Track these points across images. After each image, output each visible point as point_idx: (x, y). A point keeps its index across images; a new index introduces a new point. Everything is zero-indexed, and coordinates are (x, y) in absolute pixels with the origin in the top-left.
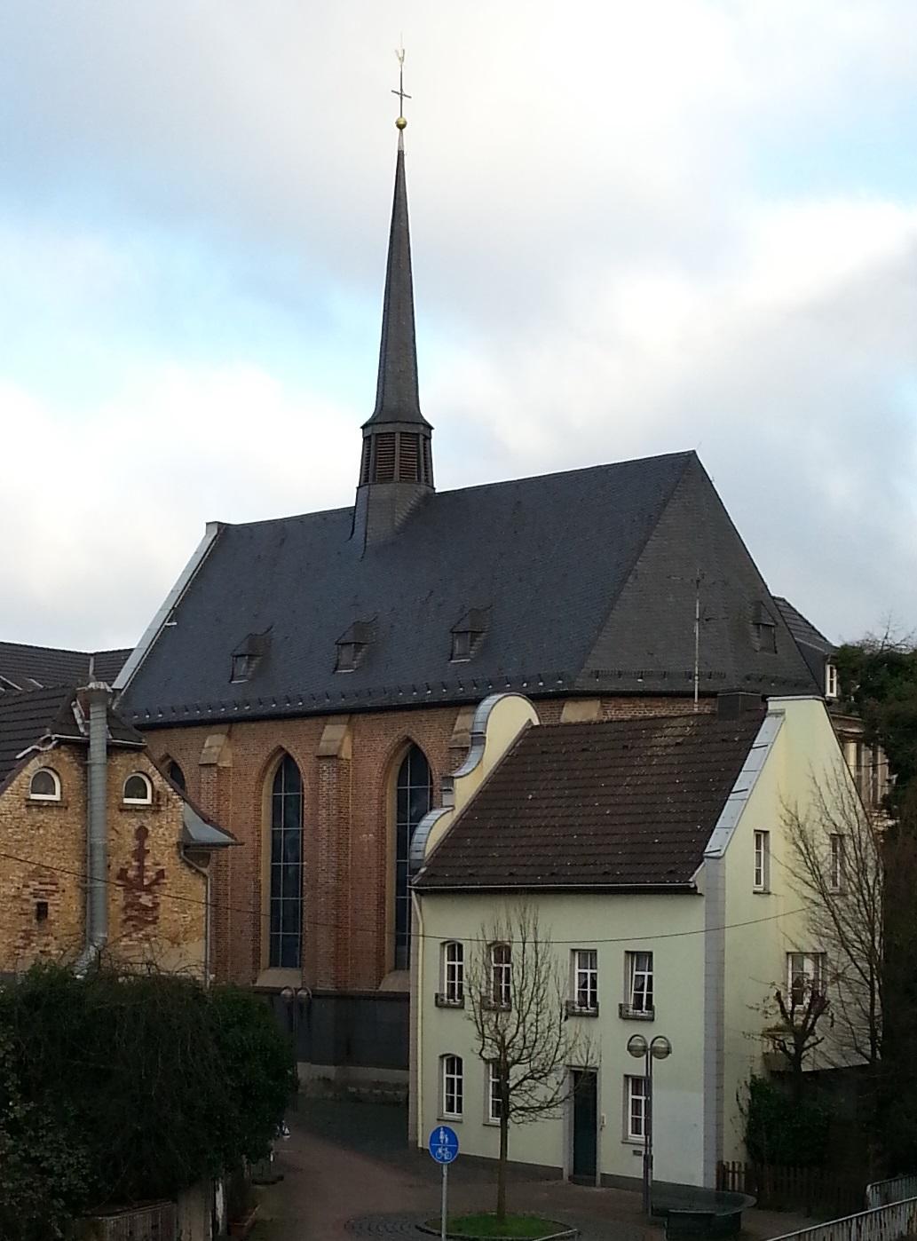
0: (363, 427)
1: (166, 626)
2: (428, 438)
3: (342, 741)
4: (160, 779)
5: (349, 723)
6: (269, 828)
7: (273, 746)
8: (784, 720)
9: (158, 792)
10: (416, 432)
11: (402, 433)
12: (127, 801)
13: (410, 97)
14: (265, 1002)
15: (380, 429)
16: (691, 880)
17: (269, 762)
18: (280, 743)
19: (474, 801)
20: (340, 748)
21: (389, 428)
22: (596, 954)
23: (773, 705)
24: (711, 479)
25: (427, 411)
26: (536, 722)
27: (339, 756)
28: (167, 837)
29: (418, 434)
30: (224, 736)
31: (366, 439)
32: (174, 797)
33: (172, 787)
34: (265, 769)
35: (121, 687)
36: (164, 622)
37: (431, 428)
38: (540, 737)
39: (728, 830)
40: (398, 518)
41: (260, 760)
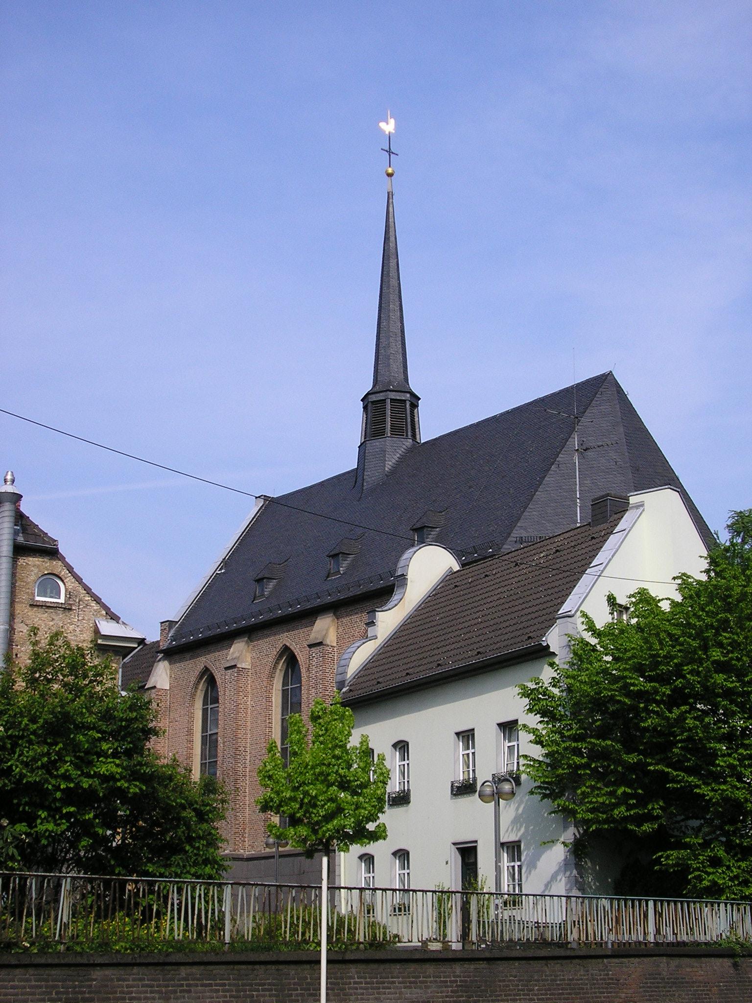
0: (362, 400)
1: (217, 574)
2: (414, 406)
3: (327, 630)
4: (73, 580)
5: (335, 614)
6: (279, 716)
7: (279, 646)
8: (644, 510)
9: (70, 592)
10: (404, 398)
11: (391, 399)
12: (37, 598)
13: (382, 149)
14: (59, 710)
15: (373, 398)
16: (544, 639)
17: (277, 663)
18: (284, 643)
19: (396, 632)
20: (325, 636)
21: (380, 397)
22: (473, 735)
23: (633, 500)
24: (626, 393)
25: (415, 384)
26: (456, 567)
27: (324, 643)
28: (78, 632)
29: (405, 401)
30: (244, 643)
31: (365, 408)
32: (87, 598)
33: (85, 590)
34: (275, 668)
35: (177, 620)
36: (216, 570)
37: (419, 399)
38: (455, 578)
39: (580, 595)
40: (388, 464)
41: (271, 659)
